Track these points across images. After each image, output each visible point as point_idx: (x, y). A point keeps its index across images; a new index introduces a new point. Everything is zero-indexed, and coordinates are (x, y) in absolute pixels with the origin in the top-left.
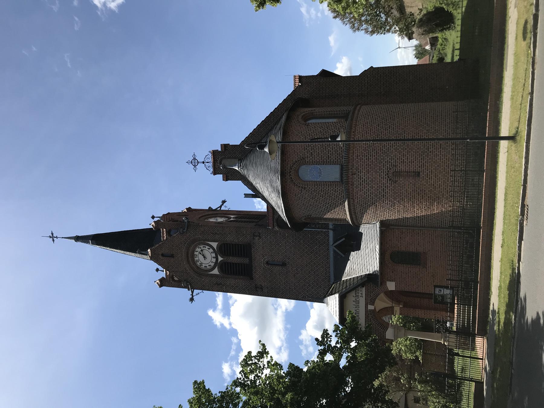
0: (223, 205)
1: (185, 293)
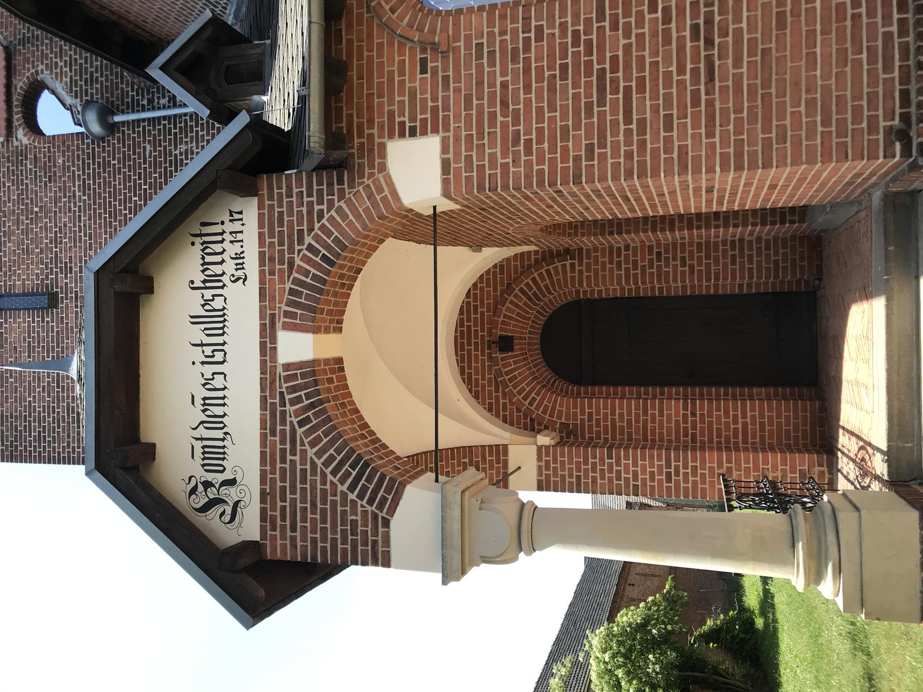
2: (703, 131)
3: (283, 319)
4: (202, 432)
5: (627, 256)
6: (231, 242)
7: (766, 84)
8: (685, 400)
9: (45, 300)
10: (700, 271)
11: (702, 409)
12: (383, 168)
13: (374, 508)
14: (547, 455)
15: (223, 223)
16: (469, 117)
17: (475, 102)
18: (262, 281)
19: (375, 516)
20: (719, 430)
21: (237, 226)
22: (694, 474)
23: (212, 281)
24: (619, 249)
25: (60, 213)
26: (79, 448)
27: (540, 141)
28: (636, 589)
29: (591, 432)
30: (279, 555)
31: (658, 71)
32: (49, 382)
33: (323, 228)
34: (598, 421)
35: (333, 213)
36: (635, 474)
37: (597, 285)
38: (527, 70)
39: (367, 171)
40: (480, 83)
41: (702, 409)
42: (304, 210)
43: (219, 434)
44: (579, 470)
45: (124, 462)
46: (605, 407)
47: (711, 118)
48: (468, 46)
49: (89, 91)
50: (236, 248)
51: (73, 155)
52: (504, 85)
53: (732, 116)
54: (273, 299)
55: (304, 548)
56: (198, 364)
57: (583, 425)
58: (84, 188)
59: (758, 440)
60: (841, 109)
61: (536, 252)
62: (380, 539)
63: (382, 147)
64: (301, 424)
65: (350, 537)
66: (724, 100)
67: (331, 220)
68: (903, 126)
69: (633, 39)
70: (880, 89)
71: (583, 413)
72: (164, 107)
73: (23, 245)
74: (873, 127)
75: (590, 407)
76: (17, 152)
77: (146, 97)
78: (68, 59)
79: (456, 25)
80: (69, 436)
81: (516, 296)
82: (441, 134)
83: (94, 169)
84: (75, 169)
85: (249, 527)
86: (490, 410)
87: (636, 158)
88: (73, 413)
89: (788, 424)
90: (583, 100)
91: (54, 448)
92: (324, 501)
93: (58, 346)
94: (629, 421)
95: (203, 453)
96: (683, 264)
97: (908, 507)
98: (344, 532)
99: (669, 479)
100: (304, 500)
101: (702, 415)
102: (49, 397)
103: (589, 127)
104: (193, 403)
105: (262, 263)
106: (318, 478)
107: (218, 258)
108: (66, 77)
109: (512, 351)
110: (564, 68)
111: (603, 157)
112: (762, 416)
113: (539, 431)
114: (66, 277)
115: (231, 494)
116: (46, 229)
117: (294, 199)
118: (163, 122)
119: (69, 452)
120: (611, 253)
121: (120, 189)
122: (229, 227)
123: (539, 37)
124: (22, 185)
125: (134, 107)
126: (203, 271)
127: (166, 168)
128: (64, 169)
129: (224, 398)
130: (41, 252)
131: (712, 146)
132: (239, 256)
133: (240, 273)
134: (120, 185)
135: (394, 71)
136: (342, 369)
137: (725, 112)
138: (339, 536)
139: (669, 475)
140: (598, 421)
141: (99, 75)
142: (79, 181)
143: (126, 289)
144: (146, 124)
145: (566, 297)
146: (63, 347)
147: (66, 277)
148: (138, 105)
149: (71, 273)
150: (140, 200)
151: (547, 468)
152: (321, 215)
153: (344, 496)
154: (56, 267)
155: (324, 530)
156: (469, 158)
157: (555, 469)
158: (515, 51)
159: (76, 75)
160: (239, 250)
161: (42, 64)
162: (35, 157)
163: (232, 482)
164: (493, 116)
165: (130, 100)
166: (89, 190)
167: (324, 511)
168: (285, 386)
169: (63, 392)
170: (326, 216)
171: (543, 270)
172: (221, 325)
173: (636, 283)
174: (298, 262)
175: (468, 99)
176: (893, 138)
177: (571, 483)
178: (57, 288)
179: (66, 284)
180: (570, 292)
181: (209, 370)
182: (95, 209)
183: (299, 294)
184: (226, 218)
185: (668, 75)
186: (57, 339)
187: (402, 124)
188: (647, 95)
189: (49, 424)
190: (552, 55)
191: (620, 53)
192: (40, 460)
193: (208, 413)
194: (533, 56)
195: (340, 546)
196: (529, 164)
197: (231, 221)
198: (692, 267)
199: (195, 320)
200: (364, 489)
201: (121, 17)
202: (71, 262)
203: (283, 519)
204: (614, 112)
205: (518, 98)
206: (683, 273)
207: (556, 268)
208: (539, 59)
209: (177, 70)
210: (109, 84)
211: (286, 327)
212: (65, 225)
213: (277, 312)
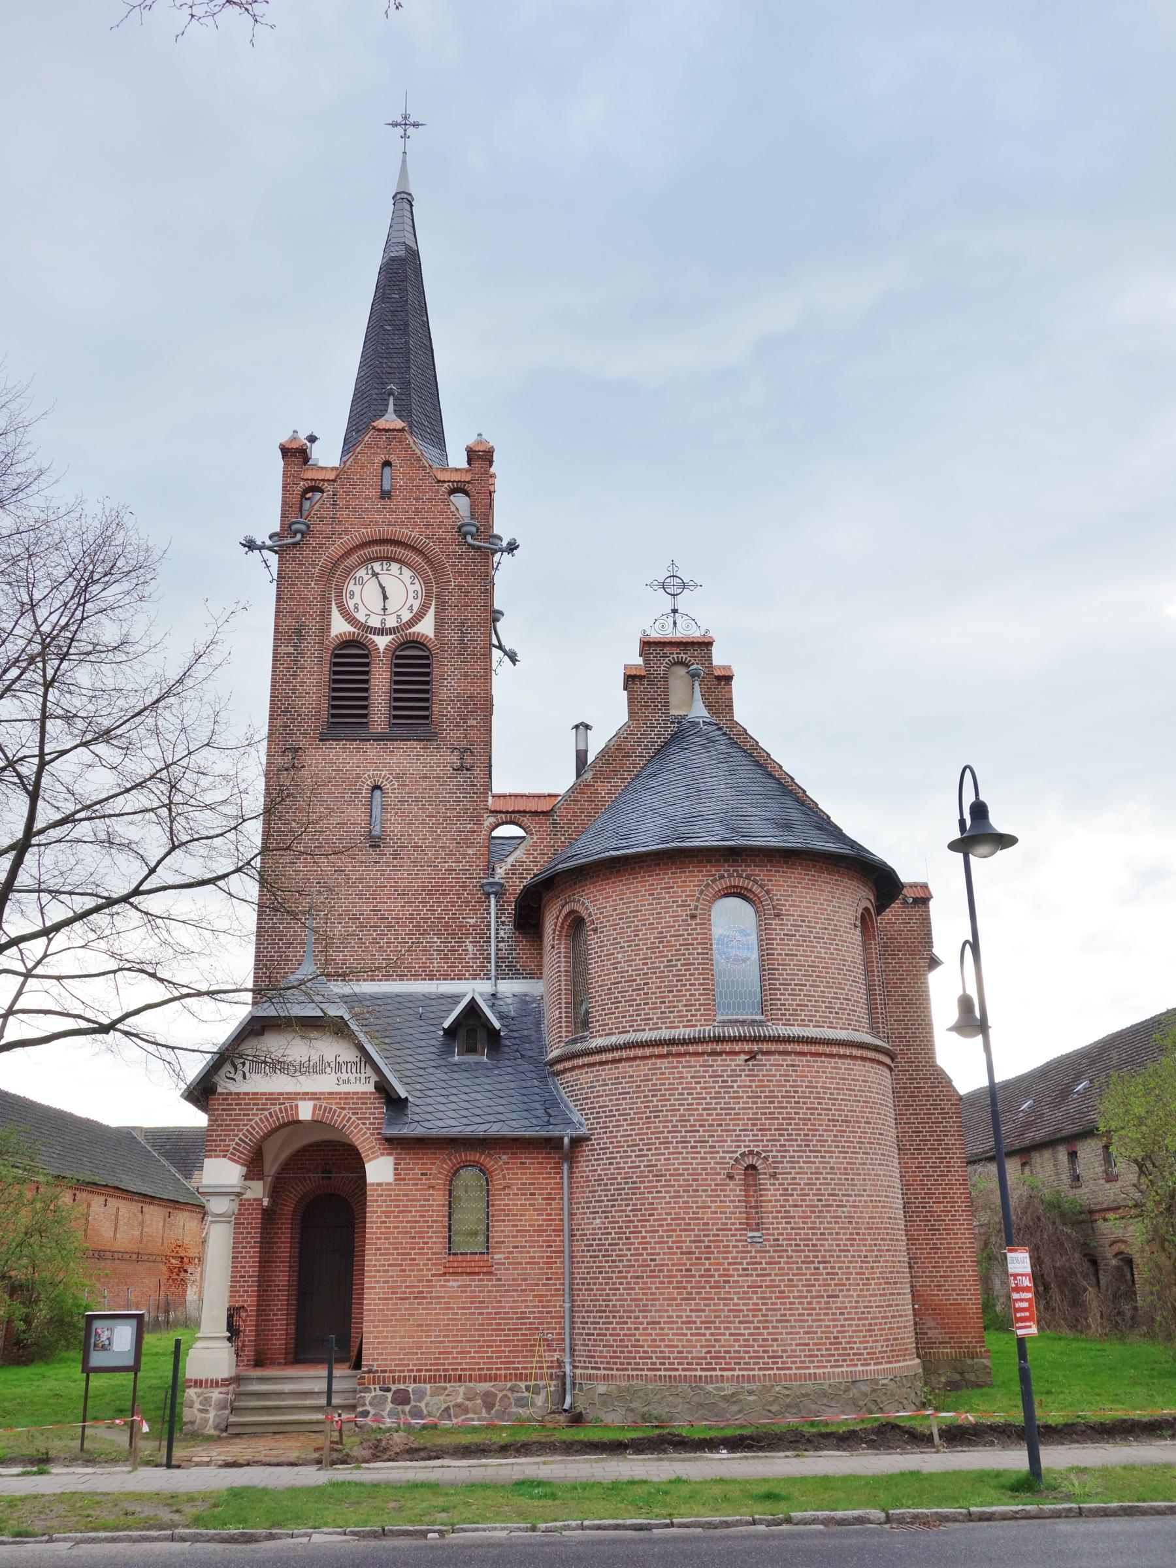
0: (506, 653)
1: (267, 520)
7: (396, 1320)
12: (382, 1154)
18: (337, 1093)
21: (363, 1080)
28: (103, 1209)
47: (385, 1299)
50: (353, 1080)
54: (328, 1099)
63: (390, 1154)
74: (374, 1360)
86: (286, 1165)
105: (345, 1093)
110: (414, 1238)
111: (375, 1254)
115: (239, 1077)
122: (363, 1076)
123: (429, 1227)
135: (416, 1166)
152: (364, 1124)
153: (237, 1135)
163: (244, 1078)
164: (398, 1206)
175: (407, 1195)
211: (315, 1106)
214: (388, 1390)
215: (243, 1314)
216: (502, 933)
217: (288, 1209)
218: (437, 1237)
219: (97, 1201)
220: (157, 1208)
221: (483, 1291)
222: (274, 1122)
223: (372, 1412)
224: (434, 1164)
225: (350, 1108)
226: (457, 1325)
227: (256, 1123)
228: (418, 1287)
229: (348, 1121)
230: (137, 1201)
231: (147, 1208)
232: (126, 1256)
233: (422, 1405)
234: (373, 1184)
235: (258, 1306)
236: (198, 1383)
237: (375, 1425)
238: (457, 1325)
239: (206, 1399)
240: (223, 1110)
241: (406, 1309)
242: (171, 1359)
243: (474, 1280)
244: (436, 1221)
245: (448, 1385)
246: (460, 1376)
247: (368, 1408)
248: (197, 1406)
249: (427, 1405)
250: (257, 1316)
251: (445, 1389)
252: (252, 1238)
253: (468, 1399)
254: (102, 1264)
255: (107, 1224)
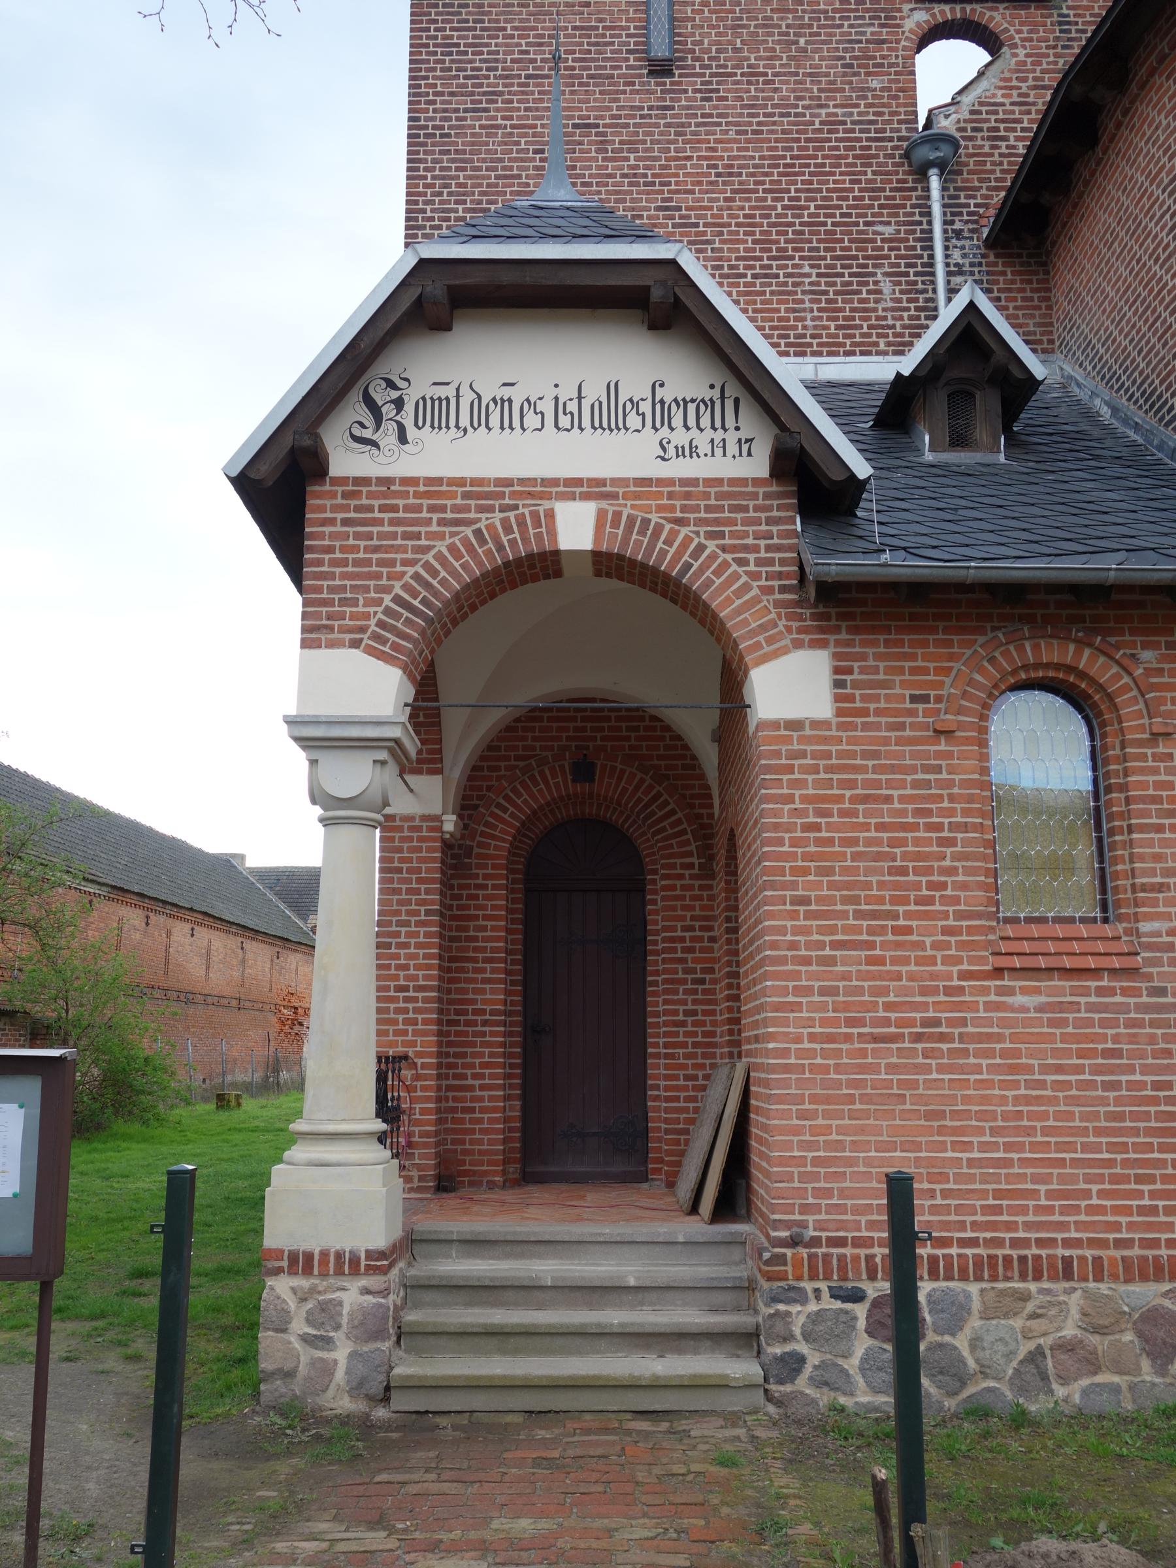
2: (818, 1030)
3: (611, 509)
4: (467, 397)
5: (701, 939)
6: (712, 441)
7: (865, 1099)
8: (505, 1013)
9: (660, 50)
10: (677, 1034)
11: (493, 1034)
12: (798, 645)
13: (373, 628)
14: (431, 829)
15: (737, 429)
16: (852, 755)
17: (870, 763)
18: (660, 482)
19: (362, 630)
20: (464, 1055)
21: (732, 448)
22: (407, 1022)
23: (662, 413)
24: (711, 929)
25: (796, 82)
26: (435, 111)
27: (819, 842)
28: (188, 940)
29: (461, 887)
30: (311, 502)
31: (891, 980)
32: (535, 61)
33: (725, 565)
34: (476, 897)
35: (744, 579)
36: (406, 945)
37: (664, 899)
38: (905, 827)
39: (795, 624)
40: (893, 769)
41: (493, 1034)
42: (750, 541)
43: (464, 421)
44: (409, 871)
45: (433, 302)
46: (494, 907)
47: (831, 1038)
48: (939, 755)
49: (979, 135)
50: (704, 448)
51: (883, 105)
52: (888, 799)
53: (831, 1062)
54: (637, 496)
55: (321, 536)
56: (555, 391)
57: (470, 877)
58: (832, 123)
59: (451, 1104)
60: (829, 1177)
61: (711, 816)
62: (336, 635)
63: (822, 644)
64: (478, 533)
65: (336, 597)
66: (851, 1054)
67: (736, 576)
68: (807, 1239)
69: (929, 952)
70: (849, 1217)
71: (486, 877)
72: (947, 256)
73: (748, 19)
74: (805, 1209)
75: (494, 887)
76: (892, 10)
77: (966, 228)
78: (1031, 100)
79: (967, 741)
80: (452, 94)
81: (651, 787)
82: (834, 720)
83: (859, 140)
84: (862, 109)
85: (346, 461)
86: (490, 748)
87: (790, 953)
88: (488, 102)
89: (472, 1142)
90: (863, 894)
91: (434, 69)
92: (381, 563)
93: (590, 77)
94: (475, 939)
95: (440, 399)
96: (687, 1013)
97: (391, 1241)
98: (343, 589)
99: (400, 989)
100: (381, 536)
101: (484, 1034)
102: (513, 61)
103: (831, 900)
104: (505, 385)
105: (685, 482)
106: (409, 556)
107: (692, 422)
108: (1003, 96)
109: (574, 781)
110: (903, 871)
111: (794, 915)
112: (483, 1110)
113: (460, 817)
114: (695, 91)
115: (387, 437)
116: (771, 58)
117: (764, 527)
118: (925, 254)
119: (427, 94)
120: (706, 918)
121: (828, 182)
122: (732, 437)
123: (942, 842)
124: (841, 18)
125: (951, 208)
126: (675, 400)
127: (856, 258)
128: (862, 89)
129: (511, 428)
130: (736, 50)
131: (798, 1039)
132: (693, 450)
133: (672, 452)
134: (835, 182)
135: (903, 672)
136: (547, 577)
137: (838, 1053)
138: (337, 582)
139: (405, 989)
140: (476, 897)
141: (1004, 150)
142: (844, 115)
143: (657, 304)
144: (925, 226)
145: (648, 855)
146: (588, 84)
147: (695, 91)
148: (953, 214)
149: (703, 99)
150: (809, 216)
151: (411, 829)
152: (742, 562)
153: (387, 590)
154: (712, 75)
155: (344, 563)
156: (802, 754)
157: (411, 839)
158: (928, 813)
159: (1005, 112)
160: (701, 451)
161: (1027, 55)
162: (883, 42)
163: (403, 439)
164: (851, 784)
165: (963, 201)
166: (829, 131)
167: (368, 562)
168: (526, 511)
169: (519, 85)
170: (740, 570)
171: (685, 825)
172: (605, 425)
173: (664, 950)
174: (684, 531)
175: (875, 755)
176: (795, 1229)
177: (391, 860)
178: (680, 76)
179: (686, 91)
180: (654, 862)
181: (547, 407)
182: (798, 140)
183: (642, 532)
184: (744, 434)
185: (885, 991)
186: (600, 76)
187: (849, 671)
188: (864, 968)
189: (471, 61)
190: (918, 857)
191: (914, 938)
192: (416, 46)
193: (492, 405)
194: (921, 834)
195: (325, 583)
196: (790, 828)
197: (740, 440)
198: (683, 1024)
199: (613, 389)
200: (396, 616)
201: (1075, 206)
202: (720, 99)
203: (358, 509)
204: (847, 929)
205: (872, 816)
206: (676, 1013)
207: (687, 843)
208: (917, 842)
209: (969, 325)
210: (988, 167)
211: (601, 515)
212: (776, 90)
213: (621, 501)
214: (857, 1296)
215: (407, 1074)
216: (957, 256)
217: (499, 846)
218: (968, 871)
219: (180, 930)
220: (261, 945)
221: (1114, 1023)
222: (488, 558)
223: (813, 1358)
224: (947, 671)
225: (700, 522)
226: (1044, 1116)
227: (439, 557)
228: (924, 1006)
229: (696, 554)
230: (235, 934)
231: (248, 945)
232: (224, 1001)
233: (961, 1342)
234: (775, 724)
235: (439, 1054)
236: (301, 1263)
237: (823, 1398)
238: (1044, 1116)
239: (324, 1307)
240: (346, 522)
241: (891, 1068)
242: (28, 1372)
243: (1086, 992)
244: (965, 828)
245: (1033, 1287)
246: (1067, 1262)
247: (802, 1348)
248: (299, 1326)
249: (975, 1343)
250: (439, 1077)
251: (1025, 1297)
252: (423, 902)
253: (1098, 1330)
254: (191, 1010)
255: (196, 960)
